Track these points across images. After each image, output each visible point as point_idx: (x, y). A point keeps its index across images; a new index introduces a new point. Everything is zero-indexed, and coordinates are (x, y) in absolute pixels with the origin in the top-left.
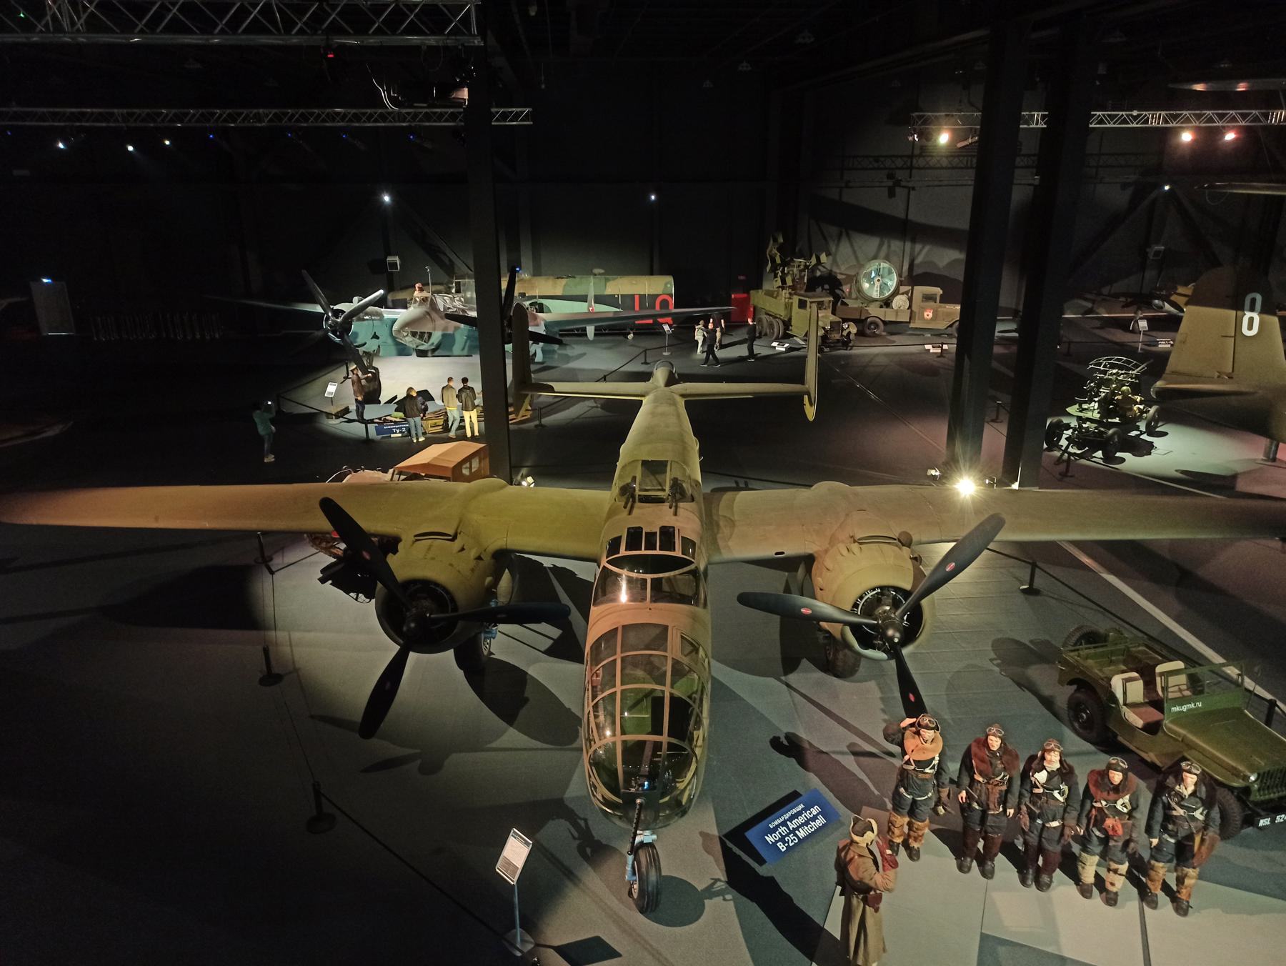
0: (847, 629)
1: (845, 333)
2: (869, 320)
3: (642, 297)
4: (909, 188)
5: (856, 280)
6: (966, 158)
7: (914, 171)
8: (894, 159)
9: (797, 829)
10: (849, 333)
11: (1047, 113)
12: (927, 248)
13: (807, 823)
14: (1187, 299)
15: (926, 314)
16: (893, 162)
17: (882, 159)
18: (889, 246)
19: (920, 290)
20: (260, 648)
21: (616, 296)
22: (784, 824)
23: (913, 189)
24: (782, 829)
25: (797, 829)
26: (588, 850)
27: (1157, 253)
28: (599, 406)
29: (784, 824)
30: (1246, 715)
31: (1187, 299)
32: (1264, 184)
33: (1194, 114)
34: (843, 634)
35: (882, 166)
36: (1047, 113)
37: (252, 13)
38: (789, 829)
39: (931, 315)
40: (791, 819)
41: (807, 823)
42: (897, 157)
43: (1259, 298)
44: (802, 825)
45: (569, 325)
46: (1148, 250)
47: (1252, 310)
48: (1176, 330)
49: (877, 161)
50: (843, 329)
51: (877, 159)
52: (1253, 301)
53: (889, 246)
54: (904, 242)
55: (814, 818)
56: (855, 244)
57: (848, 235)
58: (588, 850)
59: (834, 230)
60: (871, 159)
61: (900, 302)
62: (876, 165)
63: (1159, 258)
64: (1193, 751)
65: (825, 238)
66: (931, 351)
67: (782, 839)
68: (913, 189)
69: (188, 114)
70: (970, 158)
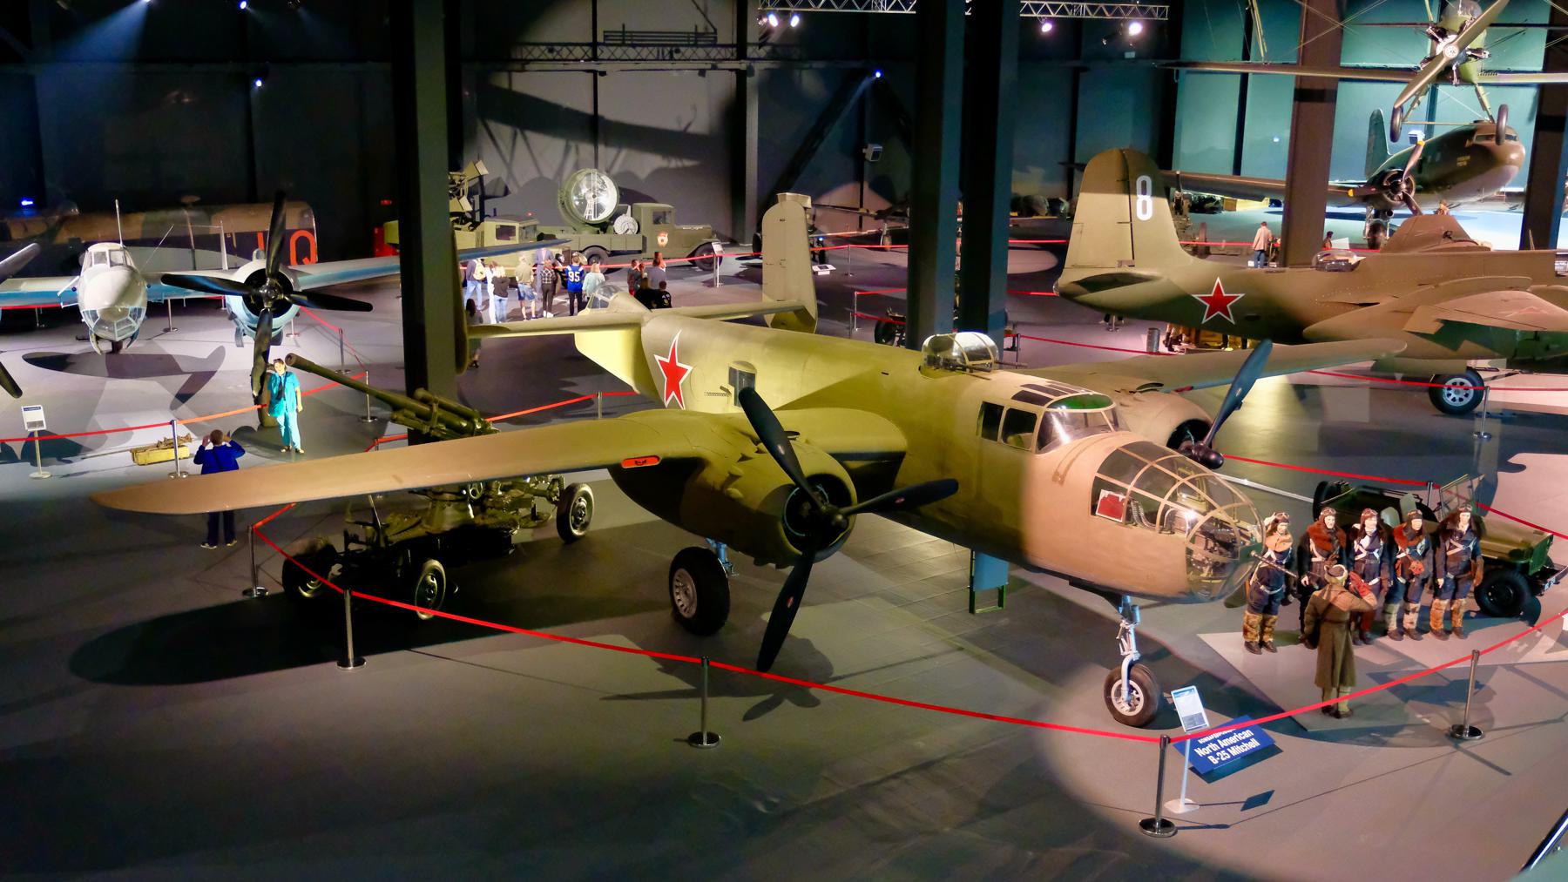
4: (595, 72)
6: (656, 48)
8: (571, 48)
9: (1229, 747)
12: (624, 153)
13: (1239, 743)
15: (659, 239)
17: (558, 48)
20: (978, 611)
22: (1214, 741)
23: (603, 74)
24: (1214, 747)
25: (1229, 747)
28: (1467, 603)
29: (1214, 741)
30: (1141, 618)
34: (1355, 630)
35: (558, 57)
38: (1219, 746)
40: (1222, 738)
41: (1239, 743)
43: (1148, 180)
44: (1234, 745)
47: (1144, 192)
49: (551, 51)
51: (551, 47)
52: (1144, 184)
55: (1247, 741)
60: (543, 48)
62: (550, 56)
63: (1228, 306)
67: (1214, 754)
68: (603, 74)
70: (661, 49)
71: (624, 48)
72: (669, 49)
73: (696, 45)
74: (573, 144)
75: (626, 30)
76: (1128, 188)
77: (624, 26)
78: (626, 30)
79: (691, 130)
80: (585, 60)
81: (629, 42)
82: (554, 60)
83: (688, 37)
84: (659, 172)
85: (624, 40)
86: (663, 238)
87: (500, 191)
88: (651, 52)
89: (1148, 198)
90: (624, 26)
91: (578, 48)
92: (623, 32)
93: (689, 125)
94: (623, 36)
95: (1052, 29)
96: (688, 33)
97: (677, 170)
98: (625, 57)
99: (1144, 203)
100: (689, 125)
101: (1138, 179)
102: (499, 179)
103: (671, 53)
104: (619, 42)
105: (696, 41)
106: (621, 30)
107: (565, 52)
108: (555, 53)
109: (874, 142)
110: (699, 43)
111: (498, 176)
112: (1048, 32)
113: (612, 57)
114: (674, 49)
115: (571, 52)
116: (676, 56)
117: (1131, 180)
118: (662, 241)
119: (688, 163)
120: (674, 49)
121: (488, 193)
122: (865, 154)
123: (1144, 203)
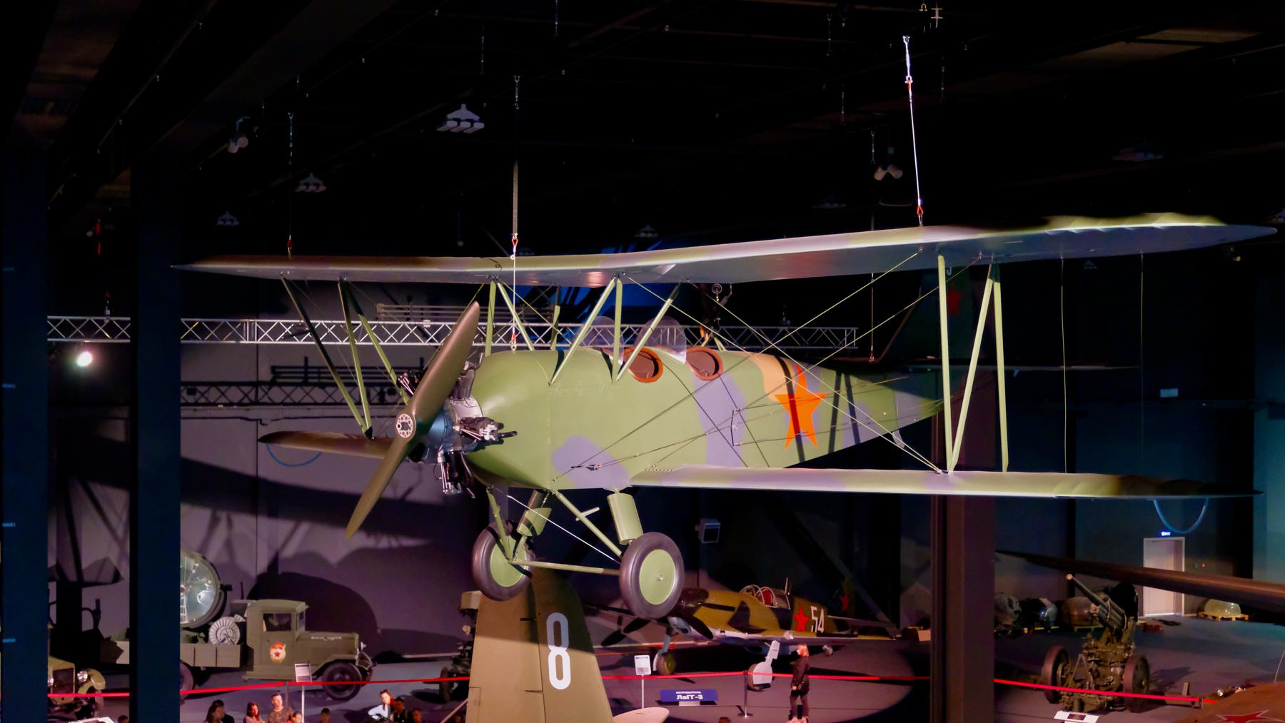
0: (569, 345)
1: (83, 691)
5: (459, 392)
7: (305, 394)
8: (223, 388)
10: (92, 690)
12: (304, 527)
15: (273, 652)
16: (223, 394)
18: (230, 524)
19: (256, 609)
27: (710, 533)
32: (937, 458)
33: (763, 330)
35: (203, 400)
37: (623, 322)
39: (283, 653)
42: (229, 384)
46: (697, 528)
47: (558, 643)
50: (79, 684)
53: (230, 524)
54: (257, 518)
63: (717, 541)
69: (778, 330)
71: (307, 389)
72: (378, 389)
73: (305, 383)
74: (223, 515)
75: (310, 364)
76: (535, 635)
77: (306, 359)
78: (310, 364)
79: (416, 496)
80: (225, 404)
81: (316, 381)
82: (196, 404)
83: (319, 373)
84: (360, 555)
85: (306, 378)
86: (279, 651)
87: (108, 576)
88: (308, 394)
89: (562, 651)
90: (306, 359)
91: (234, 389)
92: (306, 367)
93: (410, 490)
94: (306, 373)
95: (91, 365)
96: (319, 368)
97: (390, 550)
98: (307, 400)
99: (559, 659)
100: (410, 490)
101: (550, 617)
102: (105, 560)
103: (381, 394)
104: (300, 381)
105: (306, 378)
106: (418, 365)
107: (213, 394)
108: (198, 395)
109: (710, 516)
110: (311, 381)
111: (101, 557)
112: (79, 368)
113: (288, 401)
114: (386, 389)
115: (223, 394)
116: (388, 398)
117: (538, 618)
118: (277, 654)
119: (408, 542)
120: (386, 389)
121: (88, 577)
122: (697, 532)
123: (559, 659)
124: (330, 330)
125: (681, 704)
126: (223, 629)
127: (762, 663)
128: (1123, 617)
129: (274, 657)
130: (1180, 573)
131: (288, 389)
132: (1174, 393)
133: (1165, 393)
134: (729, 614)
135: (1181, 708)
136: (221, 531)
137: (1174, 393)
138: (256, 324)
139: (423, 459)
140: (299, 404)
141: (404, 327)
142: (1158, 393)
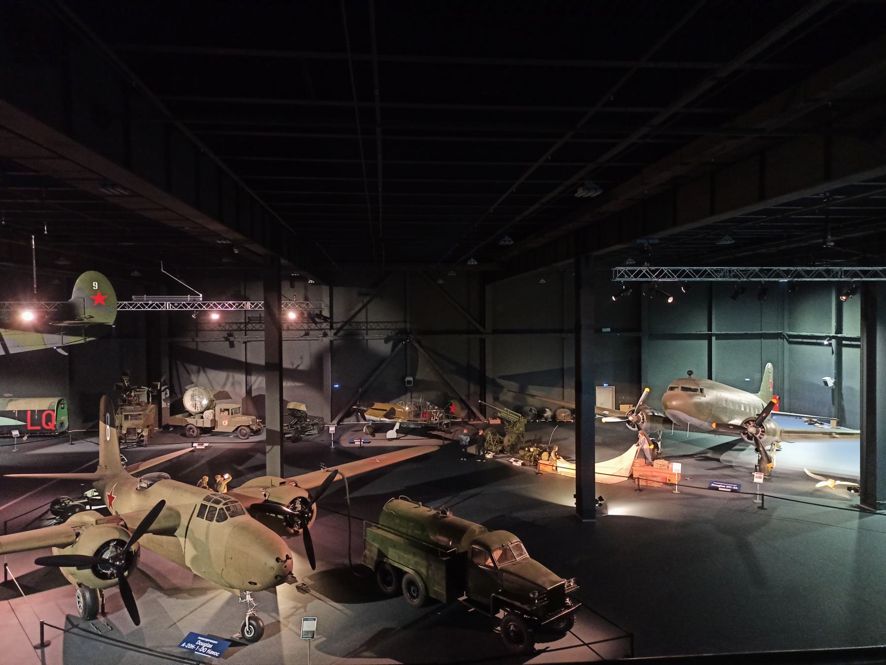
2: (188, 426)
3: (33, 412)
11: (465, 592)
14: (230, 643)
15: (223, 422)
18: (233, 377)
21: (14, 411)
26: (689, 373)
31: (230, 643)
36: (465, 592)
39: (227, 423)
45: (724, 432)
48: (708, 379)
56: (208, 375)
57: (205, 372)
58: (689, 373)
59: (194, 368)
61: (208, 414)
64: (536, 397)
65: (188, 373)
66: (197, 447)
74: (231, 374)
79: (300, 368)
85: (260, 321)
93: (298, 366)
98: (378, 327)
100: (298, 366)
108: (222, 327)
113: (254, 329)
124: (654, 276)
125: (356, 443)
126: (208, 414)
127: (392, 431)
128: (519, 417)
129: (224, 424)
130: (861, 434)
131: (254, 325)
132: (609, 330)
133: (604, 330)
134: (385, 412)
135: (839, 509)
136: (231, 379)
137: (609, 330)
138: (170, 305)
139: (195, 347)
140: (258, 330)
141: (191, 308)
142: (602, 330)
